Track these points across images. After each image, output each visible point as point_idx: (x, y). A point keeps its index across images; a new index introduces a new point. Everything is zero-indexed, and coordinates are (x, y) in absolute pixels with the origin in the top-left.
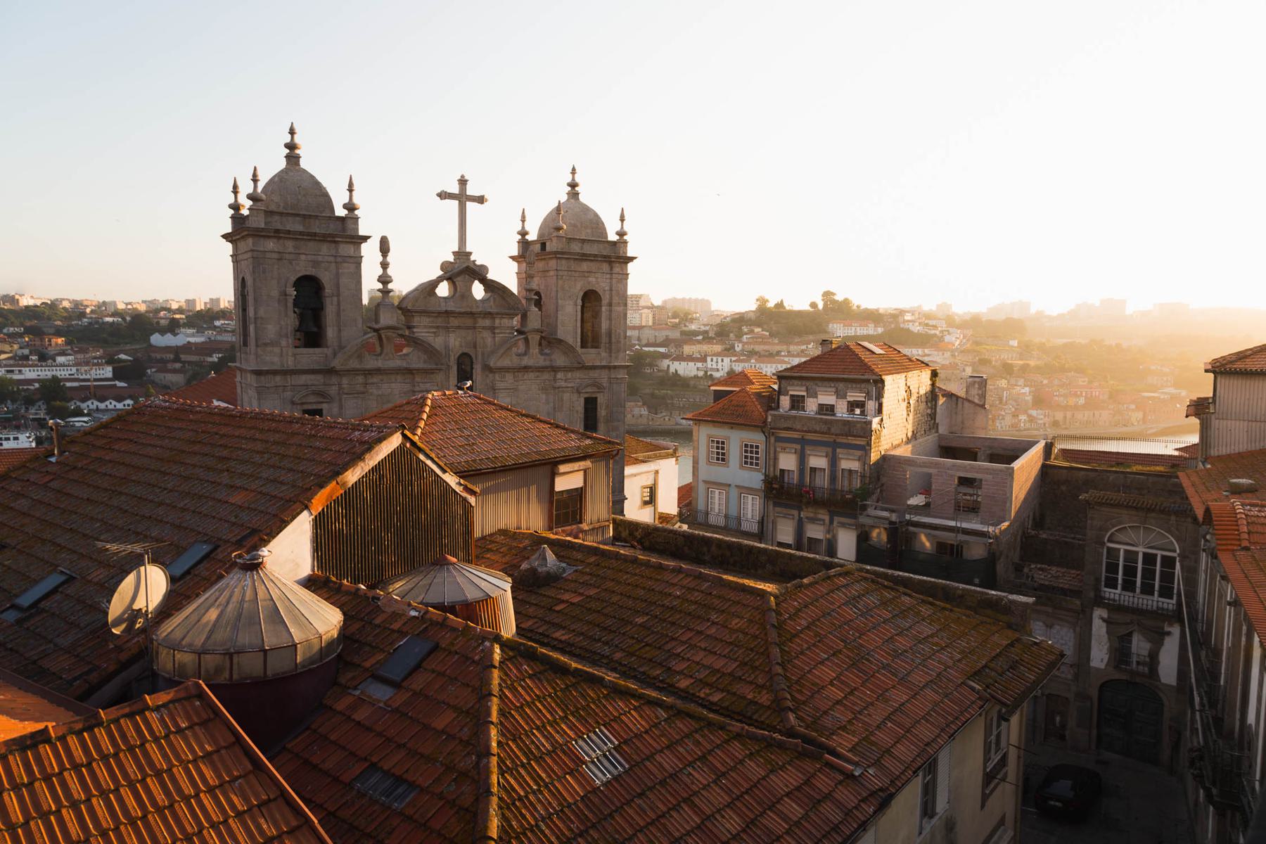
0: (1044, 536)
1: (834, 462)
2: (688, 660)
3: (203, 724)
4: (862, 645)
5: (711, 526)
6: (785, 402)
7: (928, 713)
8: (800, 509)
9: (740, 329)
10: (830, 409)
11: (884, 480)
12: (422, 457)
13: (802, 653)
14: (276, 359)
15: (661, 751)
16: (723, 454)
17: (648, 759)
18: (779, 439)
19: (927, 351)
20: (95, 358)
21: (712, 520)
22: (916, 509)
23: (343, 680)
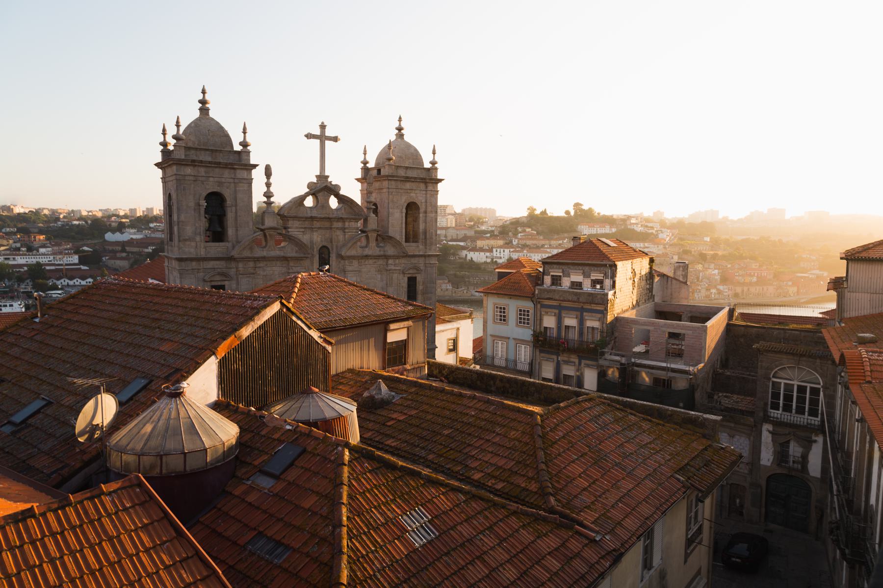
1: (581, 322)
3: (142, 504)
4: (601, 449)
5: (496, 366)
6: (548, 280)
7: (647, 497)
8: (558, 355)
9: (516, 229)
10: (579, 285)
11: (616, 334)
12: (294, 318)
13: (559, 455)
14: (192, 250)
15: (461, 523)
16: (504, 316)
17: (452, 529)
18: (543, 306)
19: (646, 245)
20: (66, 249)
21: (497, 362)
22: (639, 355)
23: (239, 474)
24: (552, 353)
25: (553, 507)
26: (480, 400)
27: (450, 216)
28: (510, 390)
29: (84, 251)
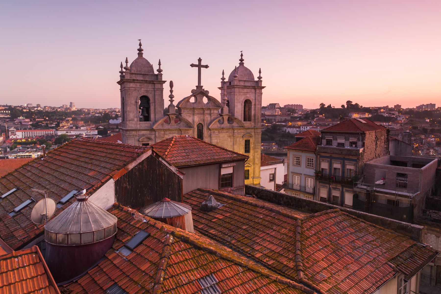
0: (436, 199)
1: (343, 166)
2: (262, 245)
3: (34, 264)
5: (294, 190)
6: (324, 142)
7: (367, 276)
8: (330, 184)
9: (314, 116)
10: (342, 145)
12: (160, 159)
13: (311, 245)
14: (133, 126)
15: (238, 286)
16: (299, 162)
17: (231, 289)
18: (321, 157)
19: (390, 124)
21: (295, 187)
22: (379, 186)
23: (114, 247)
24: (326, 183)
25: (301, 279)
26: (267, 209)
27: (278, 109)
28: (292, 204)
29: (100, 128)
